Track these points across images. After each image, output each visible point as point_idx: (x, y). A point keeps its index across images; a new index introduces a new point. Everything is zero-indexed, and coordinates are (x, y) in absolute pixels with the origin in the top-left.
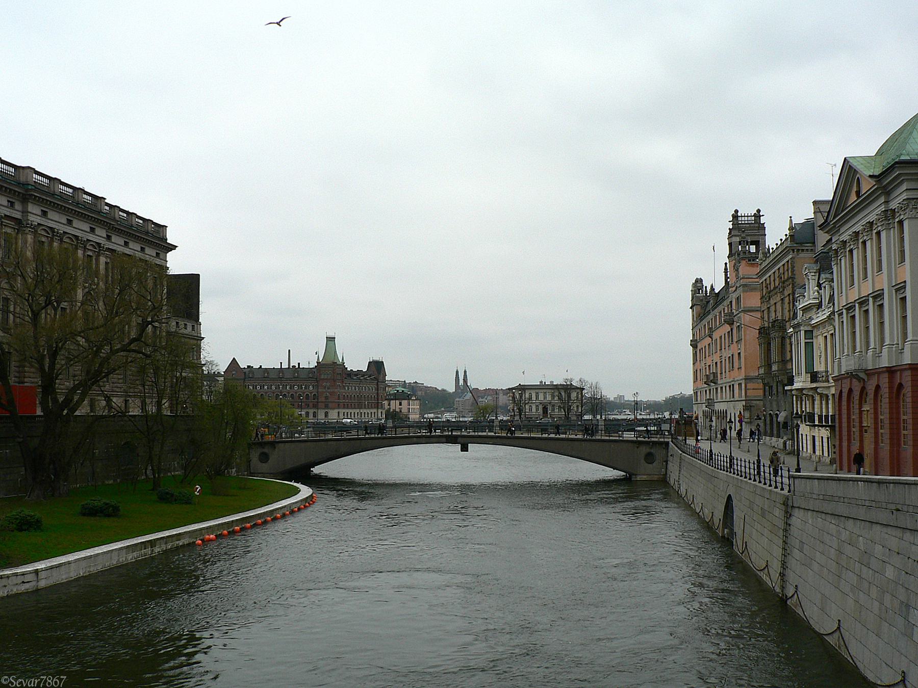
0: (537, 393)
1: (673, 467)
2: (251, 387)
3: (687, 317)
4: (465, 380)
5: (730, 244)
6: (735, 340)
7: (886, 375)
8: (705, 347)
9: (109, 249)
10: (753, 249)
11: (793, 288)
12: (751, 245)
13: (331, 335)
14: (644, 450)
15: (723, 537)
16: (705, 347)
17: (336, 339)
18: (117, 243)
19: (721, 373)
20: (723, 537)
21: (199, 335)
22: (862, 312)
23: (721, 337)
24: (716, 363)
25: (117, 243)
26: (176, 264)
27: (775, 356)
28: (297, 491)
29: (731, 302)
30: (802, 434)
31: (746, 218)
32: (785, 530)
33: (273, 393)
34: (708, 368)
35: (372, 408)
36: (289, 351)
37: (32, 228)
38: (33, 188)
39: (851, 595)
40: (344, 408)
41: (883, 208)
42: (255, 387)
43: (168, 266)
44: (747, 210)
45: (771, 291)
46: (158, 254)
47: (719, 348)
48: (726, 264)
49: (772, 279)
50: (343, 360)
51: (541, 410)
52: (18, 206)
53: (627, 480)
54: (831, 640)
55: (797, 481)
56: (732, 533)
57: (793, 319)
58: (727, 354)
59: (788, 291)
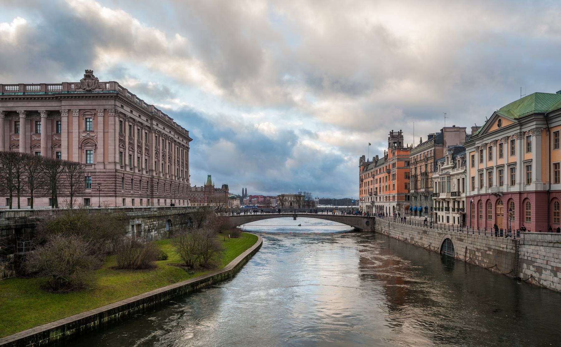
0: (288, 198)
3: (357, 170)
4: (246, 193)
7: (518, 195)
22: (498, 170)
30: (439, 216)
41: (519, 131)
44: (396, 130)
51: (289, 204)
52: (149, 121)
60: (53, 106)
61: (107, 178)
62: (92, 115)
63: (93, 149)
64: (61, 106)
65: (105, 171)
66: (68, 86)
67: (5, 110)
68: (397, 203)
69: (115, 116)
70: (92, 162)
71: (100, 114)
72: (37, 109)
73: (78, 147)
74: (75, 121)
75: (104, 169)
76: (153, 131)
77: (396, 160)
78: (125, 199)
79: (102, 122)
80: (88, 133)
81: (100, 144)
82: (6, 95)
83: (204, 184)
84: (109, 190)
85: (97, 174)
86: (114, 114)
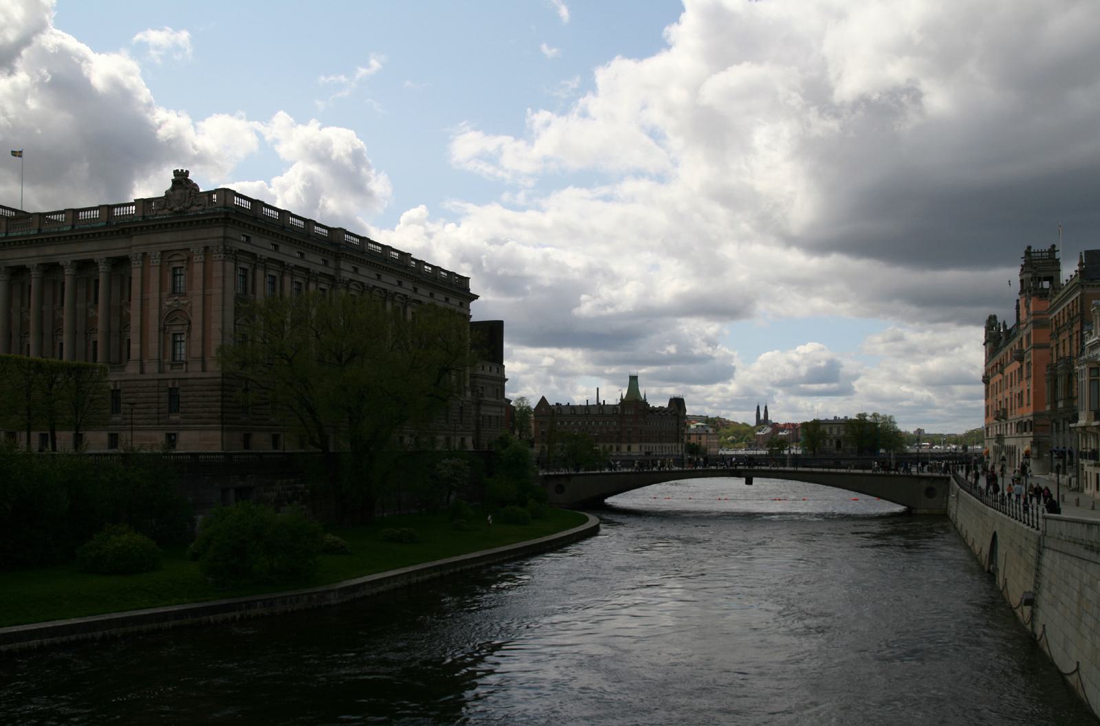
0: (831, 429)
1: (952, 503)
5: (1022, 281)
6: (1025, 376)
8: (997, 383)
9: (415, 301)
10: (1046, 284)
11: (1081, 324)
12: (1044, 280)
14: (925, 484)
15: (989, 571)
16: (997, 383)
17: (639, 379)
18: (423, 294)
19: (1011, 409)
20: (989, 571)
23: (1011, 374)
24: (1006, 399)
25: (423, 294)
27: (1061, 393)
28: (587, 520)
29: (1021, 339)
30: (1086, 472)
31: (1040, 254)
32: (1037, 570)
34: (998, 405)
35: (672, 442)
36: (598, 389)
38: (345, 247)
39: (1089, 637)
40: (646, 442)
42: (562, 423)
43: (471, 314)
45: (1060, 328)
46: (461, 304)
47: (1009, 384)
48: (1018, 301)
49: (1061, 315)
52: (332, 263)
53: (908, 515)
54: (1072, 680)
55: (1048, 521)
56: (996, 569)
57: (1081, 356)
58: (1017, 390)
59: (1076, 328)
60: (118, 247)
61: (207, 390)
62: (183, 260)
63: (185, 332)
64: (130, 247)
65: (142, 377)
66: (144, 206)
67: (41, 262)
68: (1032, 439)
70: (183, 358)
71: (198, 258)
72: (23, 264)
73: (157, 327)
74: (154, 275)
75: (160, 372)
76: (340, 285)
77: (1031, 326)
79: (201, 275)
80: (175, 298)
81: (197, 319)
82: (44, 234)
83: (620, 397)
86: (222, 256)
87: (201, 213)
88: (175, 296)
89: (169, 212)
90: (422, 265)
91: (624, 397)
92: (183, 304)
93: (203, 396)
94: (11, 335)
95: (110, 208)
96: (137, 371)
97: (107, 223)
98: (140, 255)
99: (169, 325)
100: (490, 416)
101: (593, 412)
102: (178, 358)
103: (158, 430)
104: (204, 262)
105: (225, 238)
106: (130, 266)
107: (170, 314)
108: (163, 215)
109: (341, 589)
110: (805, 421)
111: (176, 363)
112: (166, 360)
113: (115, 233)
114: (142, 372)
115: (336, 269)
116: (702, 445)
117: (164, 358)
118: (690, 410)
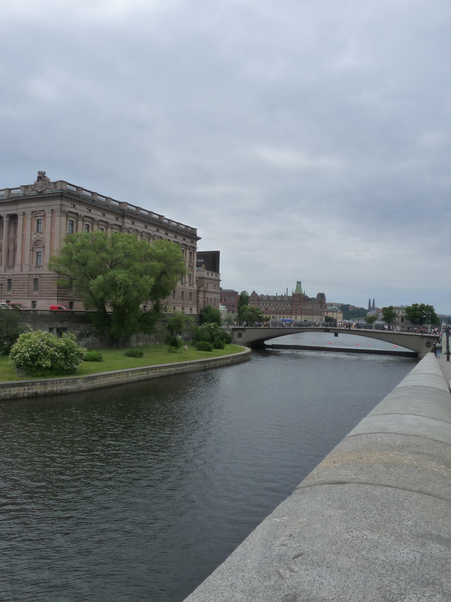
0: (399, 311)
2: (261, 304)
13: (299, 280)
17: (301, 283)
21: (219, 279)
26: (201, 246)
33: (265, 307)
36: (287, 288)
37: (127, 230)
38: (127, 212)
40: (305, 315)
43: (197, 247)
50: (304, 292)
52: (120, 219)
62: (42, 216)
63: (42, 251)
65: (22, 273)
69: (61, 216)
71: (49, 215)
73: (29, 249)
74: (28, 222)
78: (175, 307)
81: (47, 245)
83: (292, 292)
84: (53, 292)
85: (43, 276)
86: (60, 214)
87: (50, 193)
88: (37, 234)
89: (36, 192)
90: (170, 222)
91: (294, 292)
92: (42, 238)
93: (49, 283)
94: (9, 250)
95: (10, 190)
96: (20, 270)
97: (8, 197)
98: (22, 213)
99: (35, 248)
100: (211, 298)
101: (279, 299)
102: (39, 264)
103: (64, 300)
104: (51, 217)
105: (61, 205)
106: (18, 218)
107: (35, 242)
108: (33, 194)
109: (85, 378)
110: (384, 307)
111: (37, 267)
112: (33, 265)
113: (11, 202)
114: (22, 270)
115: (122, 223)
116: (334, 318)
117: (32, 264)
118: (328, 300)
